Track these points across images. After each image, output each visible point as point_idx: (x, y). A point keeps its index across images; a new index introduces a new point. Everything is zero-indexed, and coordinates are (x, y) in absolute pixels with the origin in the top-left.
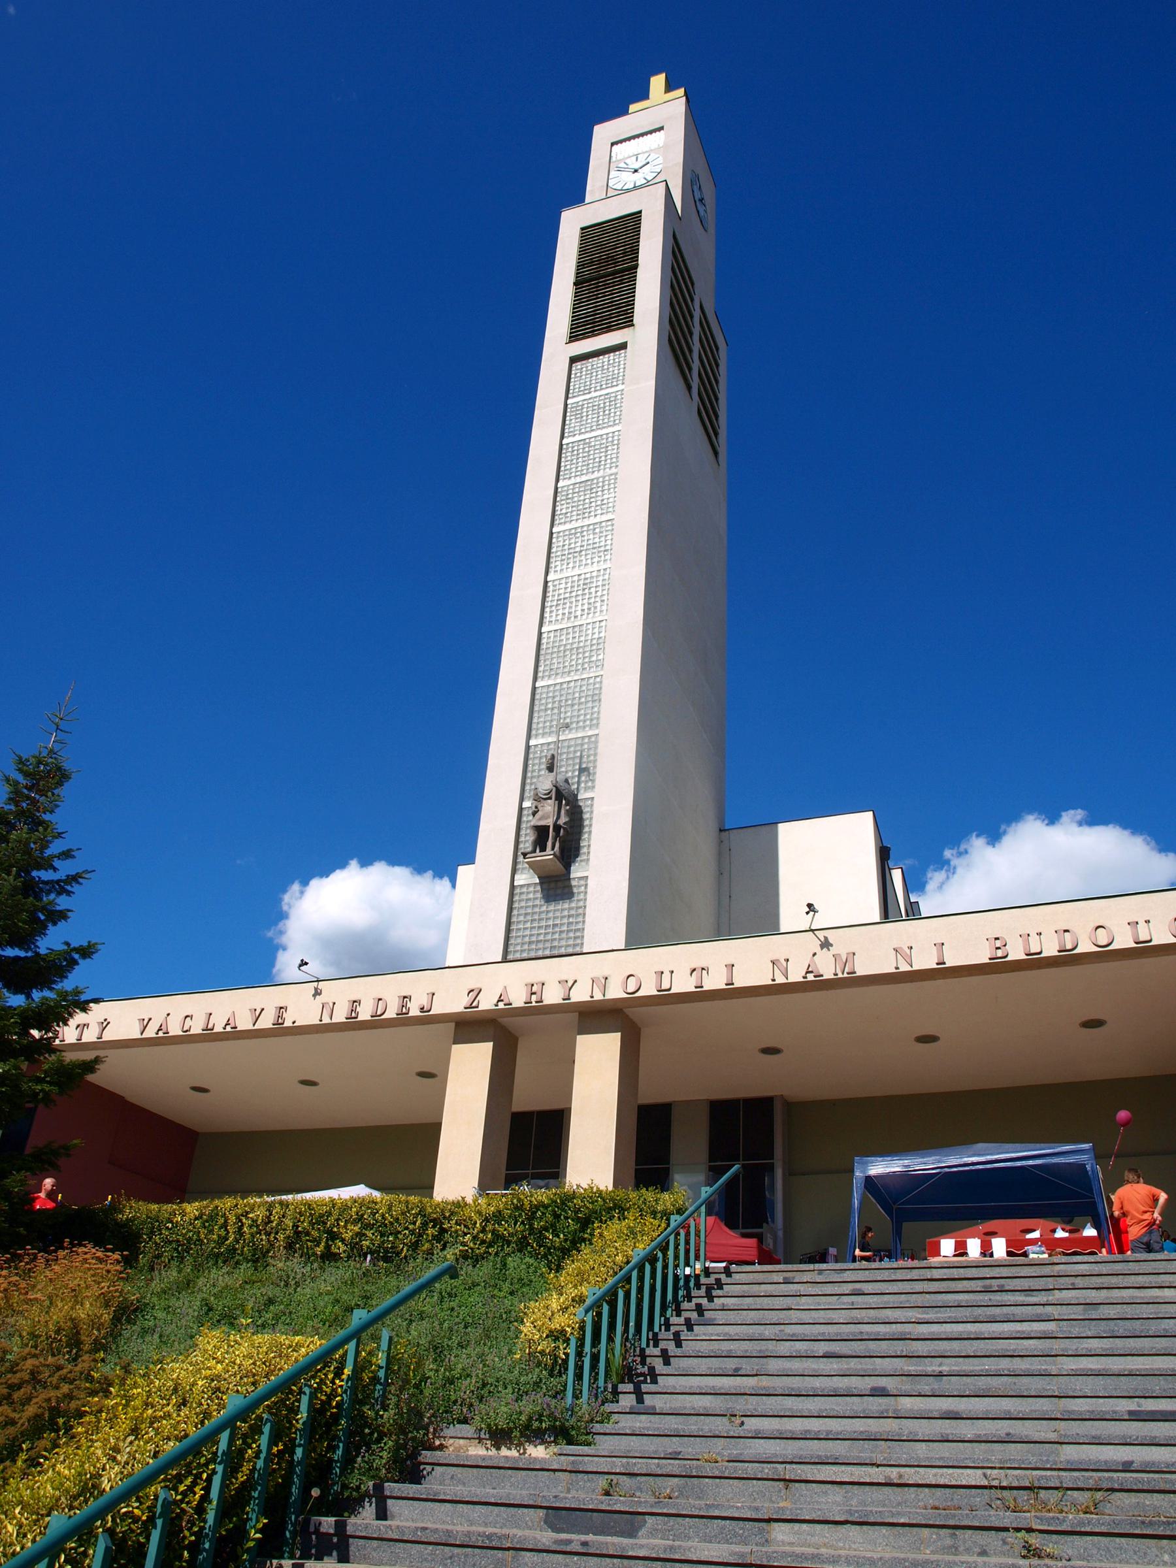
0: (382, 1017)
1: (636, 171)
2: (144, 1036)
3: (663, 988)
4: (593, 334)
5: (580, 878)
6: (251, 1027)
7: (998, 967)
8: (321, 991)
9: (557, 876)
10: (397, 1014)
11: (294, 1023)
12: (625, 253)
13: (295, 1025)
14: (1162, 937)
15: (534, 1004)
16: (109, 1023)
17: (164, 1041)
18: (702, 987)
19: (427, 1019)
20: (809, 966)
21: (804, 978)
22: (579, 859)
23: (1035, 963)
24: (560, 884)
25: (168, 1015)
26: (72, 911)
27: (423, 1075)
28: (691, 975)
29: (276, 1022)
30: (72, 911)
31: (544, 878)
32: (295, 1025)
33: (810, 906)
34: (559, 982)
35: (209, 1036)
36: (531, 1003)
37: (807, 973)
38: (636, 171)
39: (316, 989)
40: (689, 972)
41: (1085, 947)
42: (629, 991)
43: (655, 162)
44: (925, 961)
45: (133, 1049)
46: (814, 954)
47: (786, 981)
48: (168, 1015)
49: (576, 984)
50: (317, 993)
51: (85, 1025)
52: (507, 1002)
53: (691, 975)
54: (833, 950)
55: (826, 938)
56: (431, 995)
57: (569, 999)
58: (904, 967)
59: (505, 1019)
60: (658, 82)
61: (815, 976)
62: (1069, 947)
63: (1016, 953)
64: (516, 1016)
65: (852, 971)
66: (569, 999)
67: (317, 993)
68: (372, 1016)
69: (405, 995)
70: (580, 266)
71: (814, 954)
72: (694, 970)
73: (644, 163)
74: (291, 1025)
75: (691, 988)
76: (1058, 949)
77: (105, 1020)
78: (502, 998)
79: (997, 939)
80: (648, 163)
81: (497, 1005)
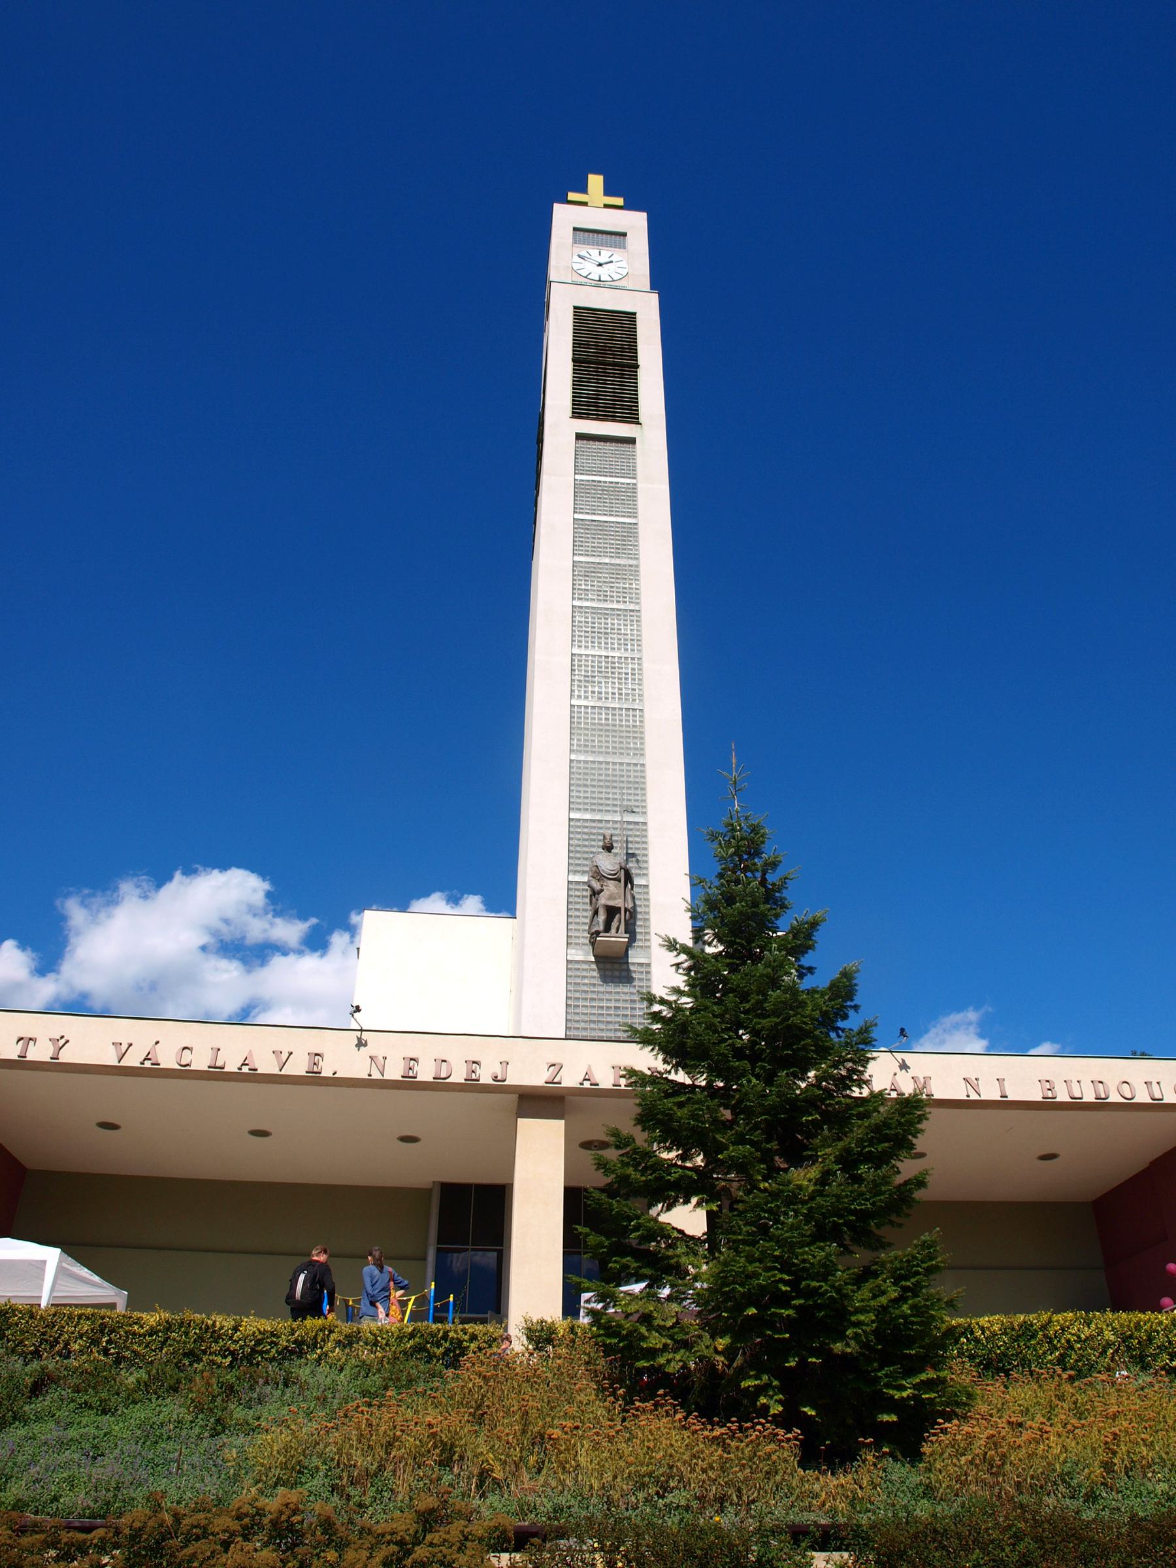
0: (447, 1081)
1: (600, 265)
2: (121, 1064)
3: (217, 1065)
4: (597, 417)
5: (641, 965)
6: (276, 1071)
7: (1048, 1106)
8: (366, 1042)
9: (614, 958)
10: (466, 1080)
11: (334, 1074)
12: (623, 349)
13: (336, 1076)
14: (1170, 1098)
15: (623, 1087)
16: (67, 1042)
17: (151, 1072)
18: (57, 1059)
19: (499, 1088)
20: (149, 1053)
21: (240, 1069)
22: (636, 944)
23: (1076, 1106)
24: (616, 966)
25: (157, 1043)
26: (676, 956)
27: (1044, 1158)
28: (17, 1043)
29: (550, 1080)
30: (676, 956)
31: (602, 957)
32: (336, 1076)
33: (902, 1030)
34: (50, 1040)
35: (216, 1074)
36: (620, 1086)
37: (243, 1065)
38: (600, 265)
39: (359, 1039)
40: (16, 1041)
41: (1114, 1098)
42: (183, 1063)
43: (619, 264)
44: (990, 1093)
45: (91, 1075)
46: (895, 1074)
47: (382, 1078)
48: (157, 1043)
49: (67, 1044)
50: (361, 1044)
51: (31, 1039)
52: (593, 1082)
53: (17, 1043)
54: (911, 1073)
55: (903, 1061)
56: (215, 1051)
57: (25, 1057)
58: (376, 1075)
59: (577, 1098)
60: (596, 182)
61: (152, 1064)
62: (443, 1075)
63: (1063, 1097)
64: (587, 1096)
65: (23, 1055)
66: (57, 1059)
67: (361, 1044)
68: (434, 1078)
69: (31, 1036)
70: (577, 345)
71: (895, 1074)
72: (554, 1065)
73: (608, 260)
74: (332, 1076)
75: (14, 1056)
76: (307, 1070)
77: (62, 1037)
78: (149, 1057)
79: (1048, 1081)
80: (611, 262)
81: (240, 1069)
